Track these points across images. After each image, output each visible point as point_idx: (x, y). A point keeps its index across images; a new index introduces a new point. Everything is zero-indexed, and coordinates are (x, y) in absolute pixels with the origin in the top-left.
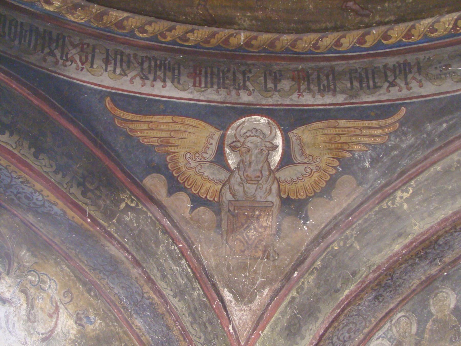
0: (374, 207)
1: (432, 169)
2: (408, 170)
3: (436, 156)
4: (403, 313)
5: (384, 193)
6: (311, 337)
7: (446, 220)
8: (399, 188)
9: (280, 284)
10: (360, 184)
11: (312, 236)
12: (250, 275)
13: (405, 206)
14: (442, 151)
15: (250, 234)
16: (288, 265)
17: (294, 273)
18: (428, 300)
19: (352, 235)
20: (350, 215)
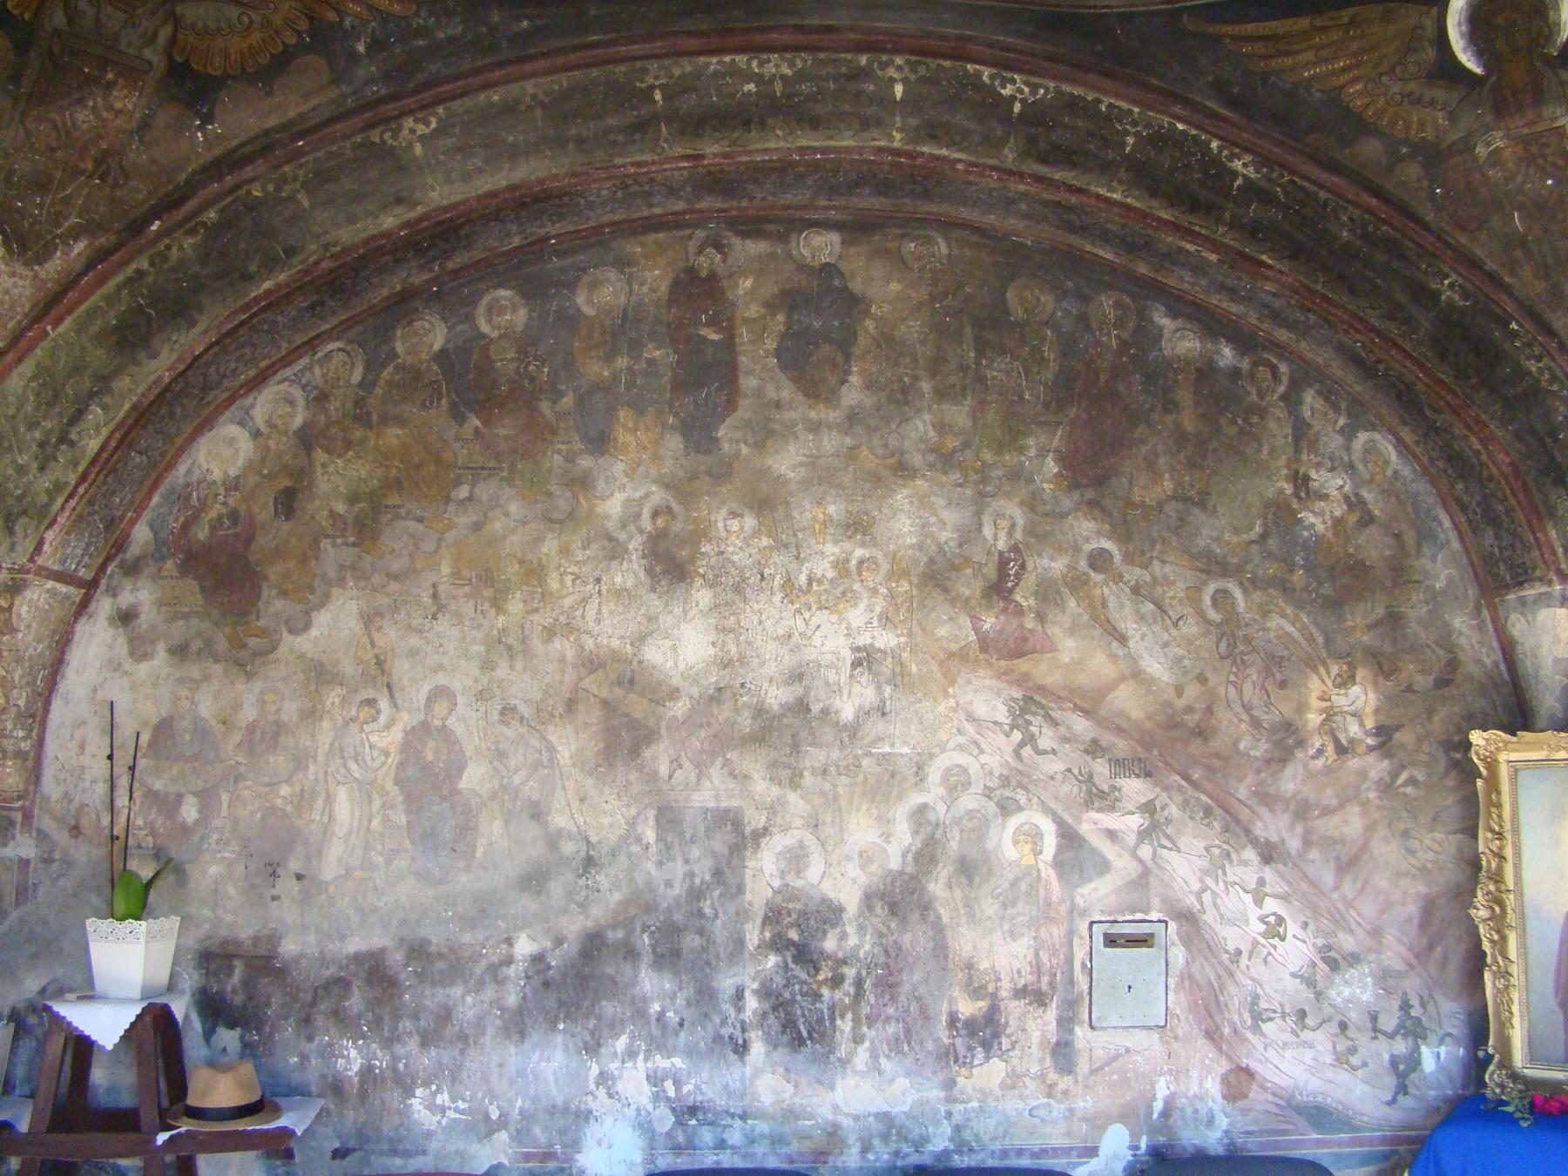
0: (353, 134)
1: (482, 97)
2: (439, 85)
3: (498, 74)
4: (339, 345)
5: (379, 112)
6: (174, 356)
7: (493, 194)
8: (411, 112)
9: (113, 239)
10: (335, 82)
11: (208, 157)
12: (53, 203)
13: (418, 149)
14: (510, 69)
15: (80, 117)
16: (143, 202)
17: (152, 223)
18: (394, 328)
19: (295, 178)
20: (301, 136)
